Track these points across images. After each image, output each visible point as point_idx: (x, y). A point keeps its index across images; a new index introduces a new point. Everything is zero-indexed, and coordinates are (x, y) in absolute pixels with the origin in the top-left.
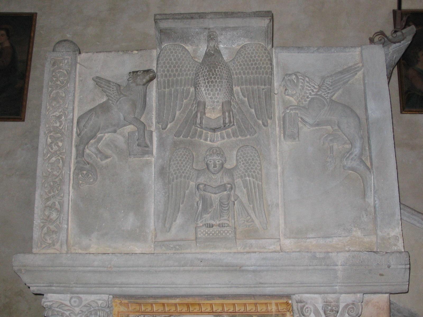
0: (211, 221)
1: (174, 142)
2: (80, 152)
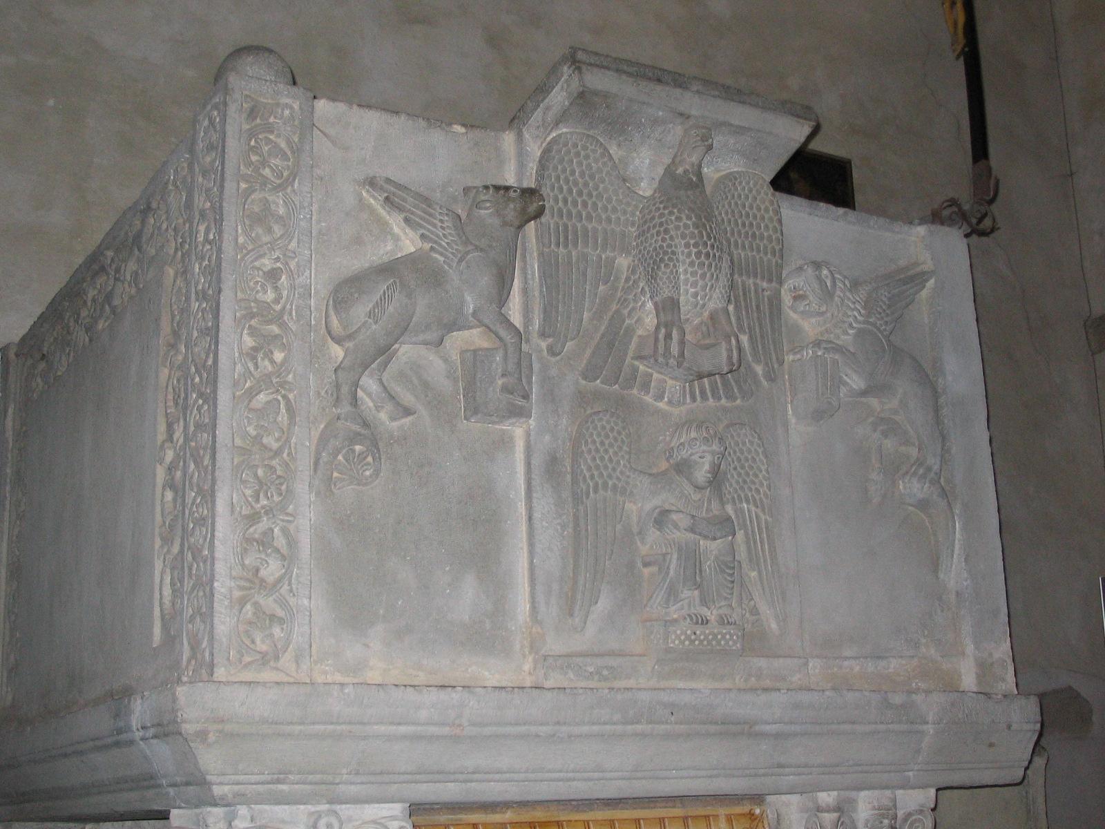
1: (580, 392)
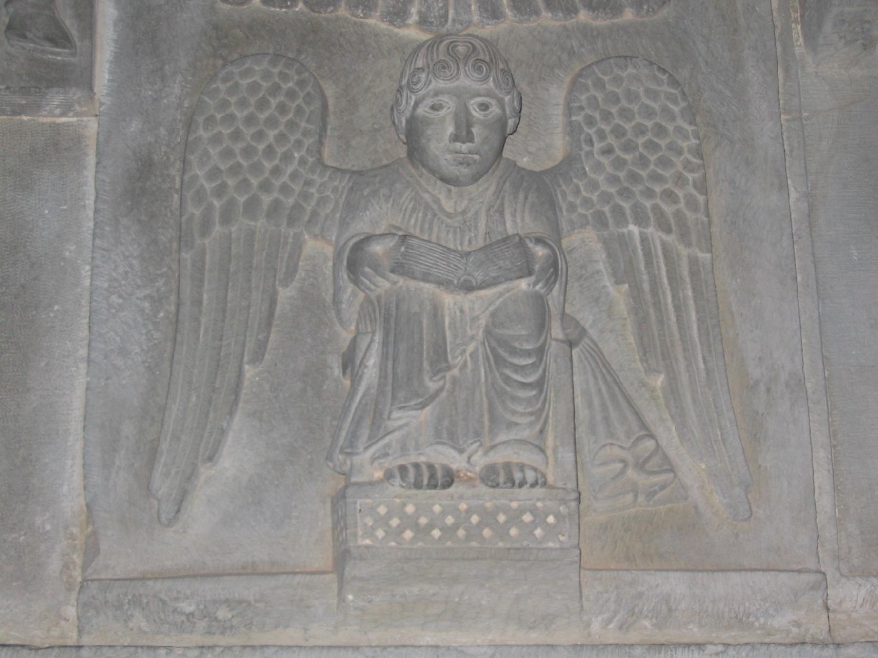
0: (440, 448)
1: (216, 28)
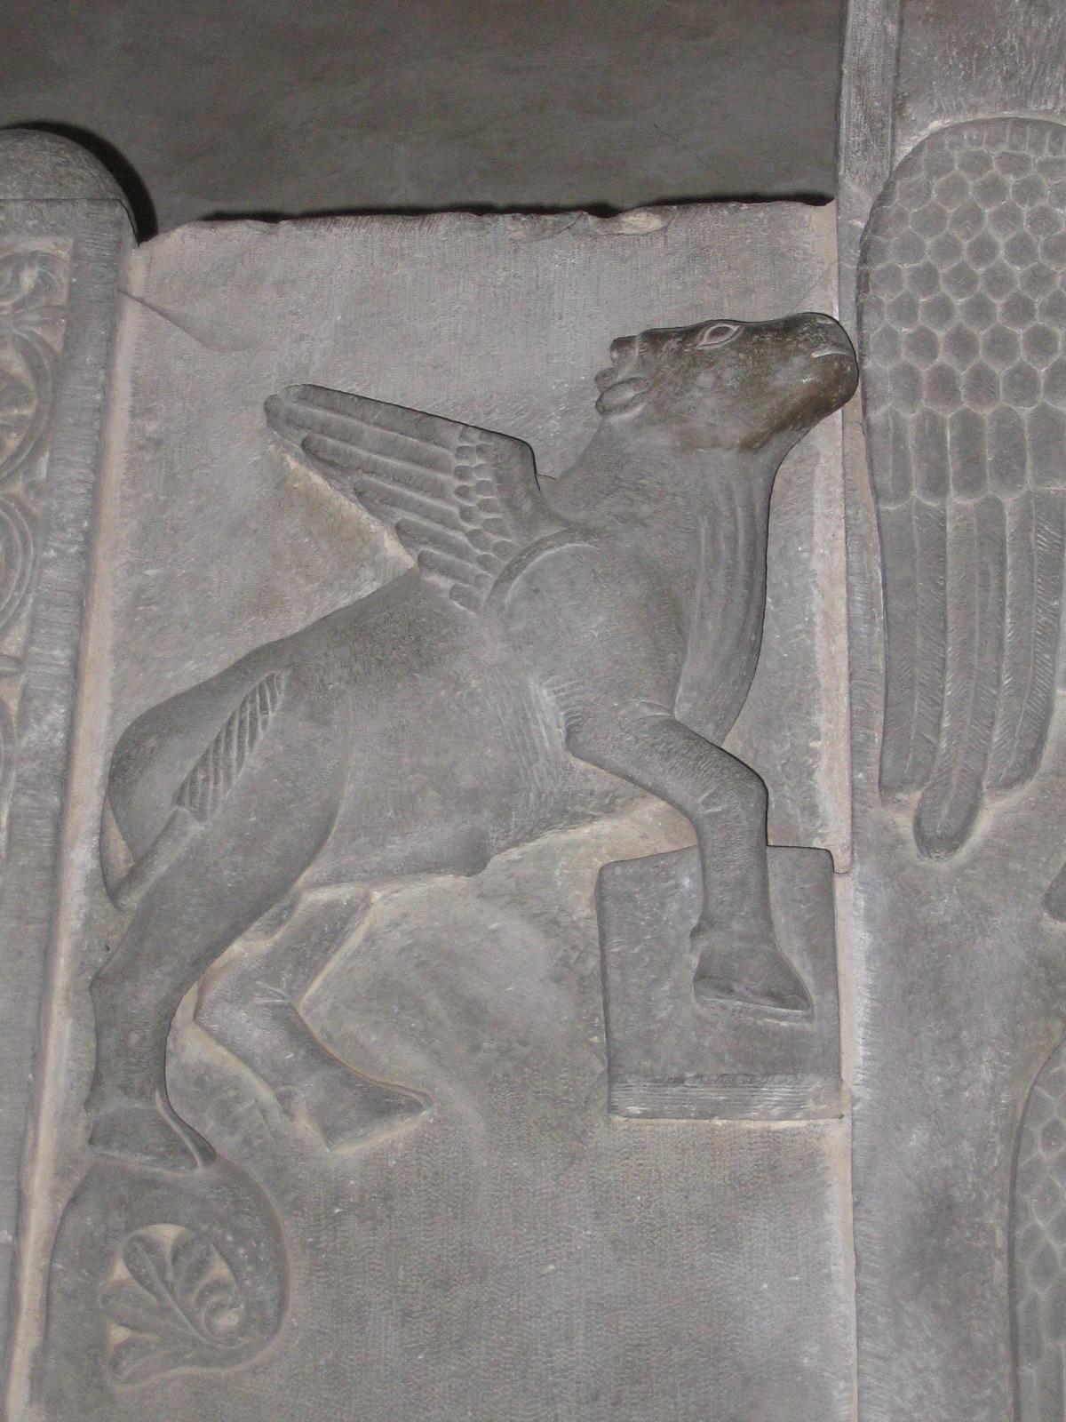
1: (1046, 963)
2: (134, 1038)
